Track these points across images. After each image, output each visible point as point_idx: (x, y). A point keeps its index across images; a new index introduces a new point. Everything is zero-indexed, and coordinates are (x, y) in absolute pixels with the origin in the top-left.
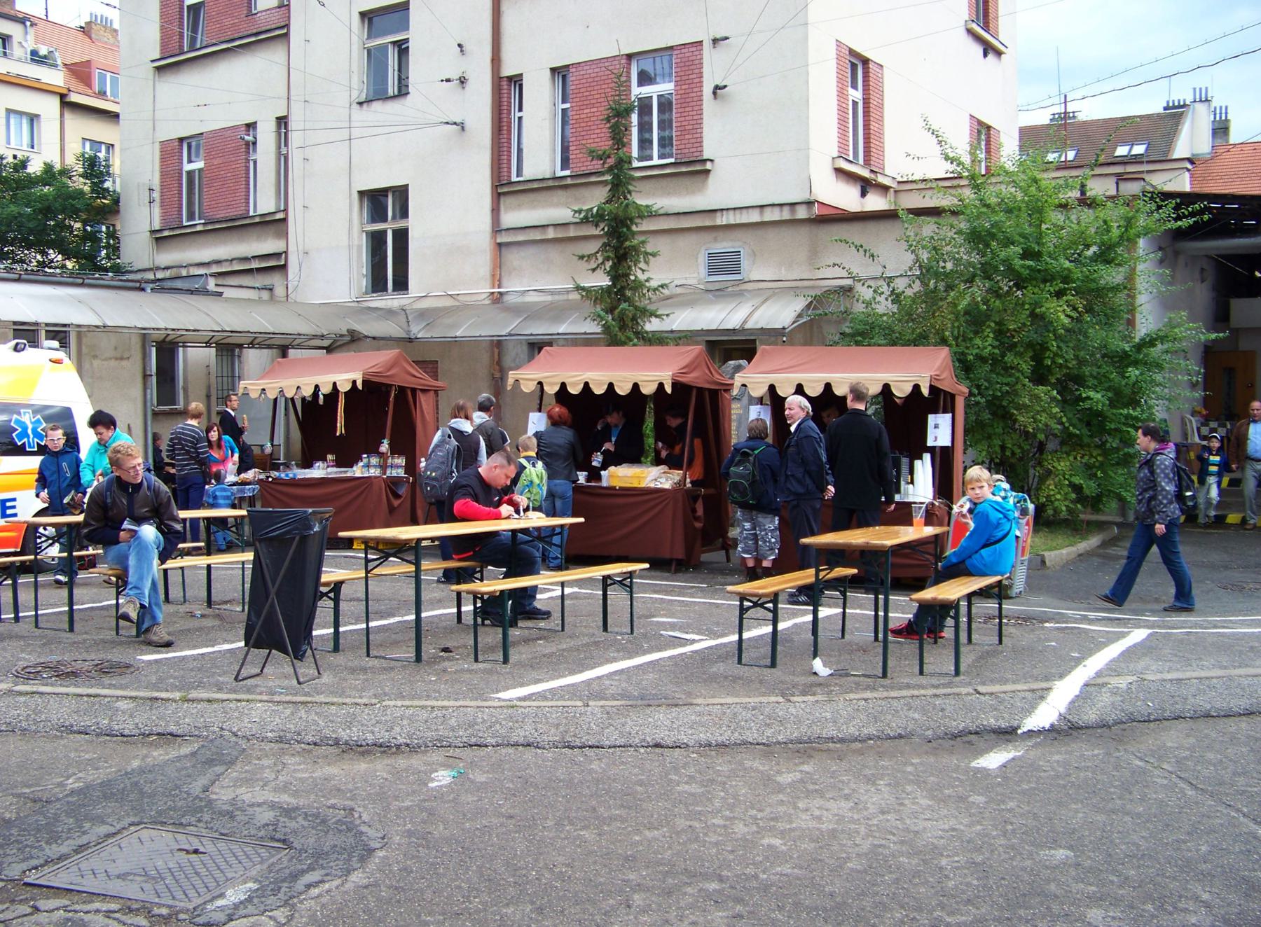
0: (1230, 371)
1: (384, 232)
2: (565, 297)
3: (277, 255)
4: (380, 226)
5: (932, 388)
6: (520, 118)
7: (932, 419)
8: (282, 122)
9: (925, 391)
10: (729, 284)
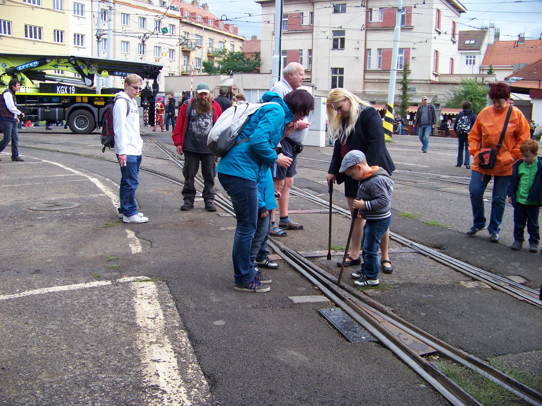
1: (336, 77)
3: (309, 79)
4: (341, 75)
6: (370, 57)
8: (310, 52)
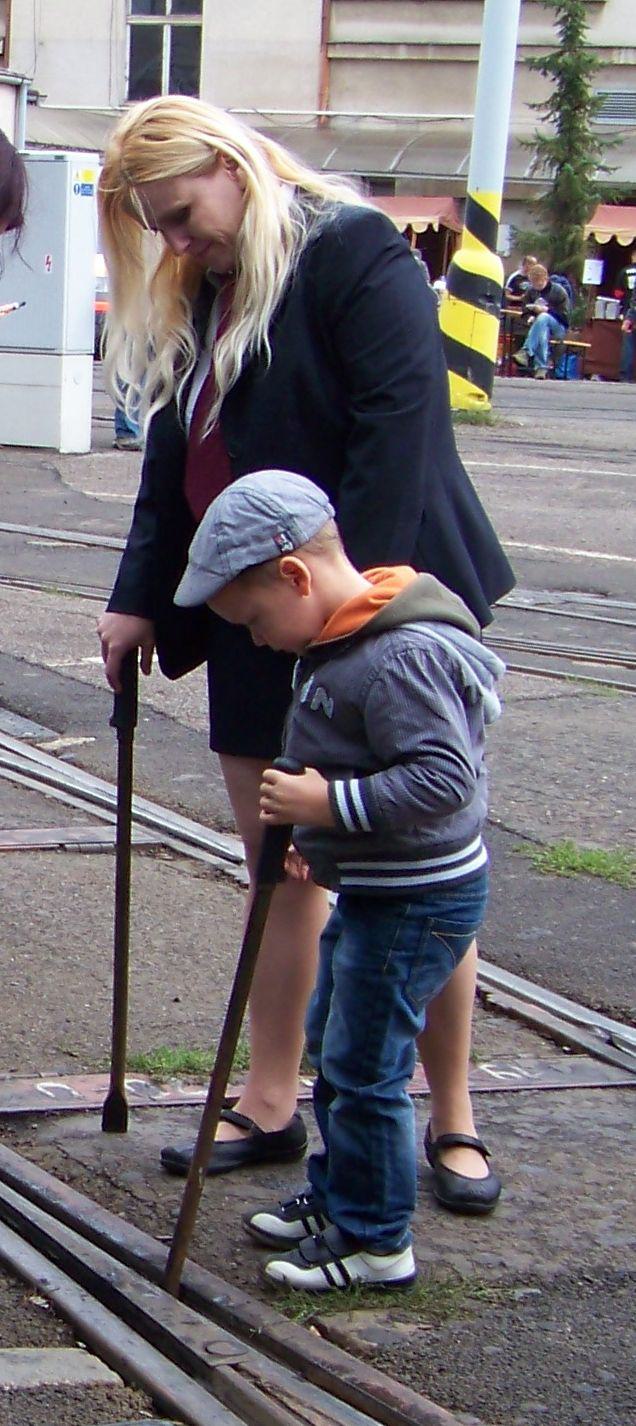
0: (559, 636)
1: (158, 29)
2: (414, 127)
5: (441, 227)
7: (597, 281)
9: (436, 228)
10: (621, 129)
